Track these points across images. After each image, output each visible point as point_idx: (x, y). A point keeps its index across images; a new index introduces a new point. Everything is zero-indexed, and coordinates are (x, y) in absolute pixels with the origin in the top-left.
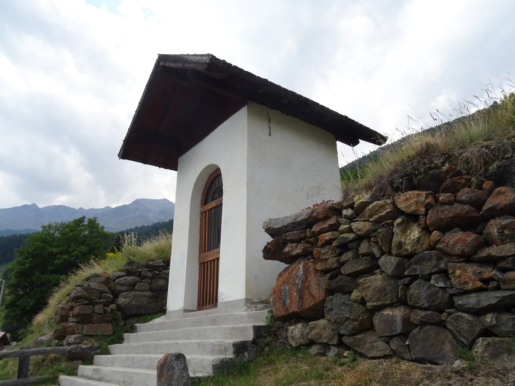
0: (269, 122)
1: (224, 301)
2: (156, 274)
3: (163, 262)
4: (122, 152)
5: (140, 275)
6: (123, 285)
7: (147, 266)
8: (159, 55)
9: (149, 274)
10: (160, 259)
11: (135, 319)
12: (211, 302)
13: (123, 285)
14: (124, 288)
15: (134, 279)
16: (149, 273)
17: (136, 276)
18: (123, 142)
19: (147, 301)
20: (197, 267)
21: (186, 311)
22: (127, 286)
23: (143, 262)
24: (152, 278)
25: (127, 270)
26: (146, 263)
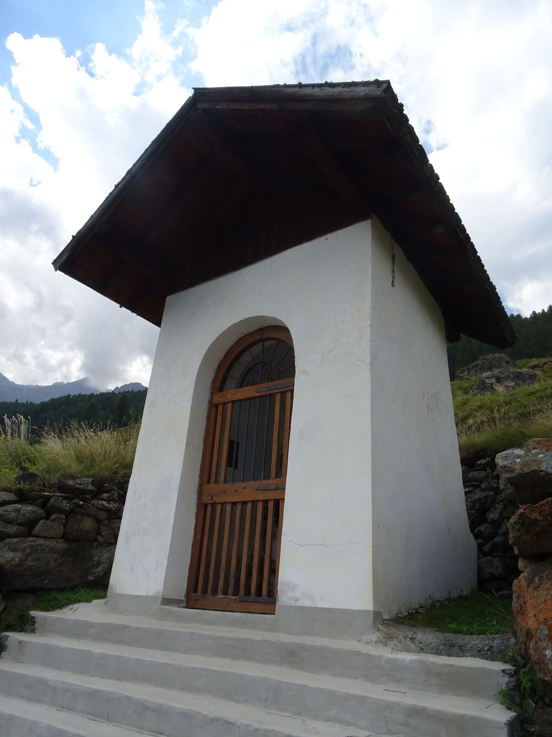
0: (393, 263)
1: (298, 604)
2: (77, 505)
3: (93, 483)
4: (64, 258)
5: (44, 503)
6: (9, 522)
7: (62, 487)
8: (195, 89)
9: (66, 505)
10: (88, 476)
11: (31, 599)
12: (231, 590)
13: (9, 522)
14: (12, 529)
15: (35, 512)
16: (65, 502)
17: (36, 505)
18: (71, 238)
19: (56, 560)
20: (194, 510)
21: (166, 601)
22: (19, 524)
23: (54, 479)
24: (69, 514)
25: (20, 490)
26: (60, 481)
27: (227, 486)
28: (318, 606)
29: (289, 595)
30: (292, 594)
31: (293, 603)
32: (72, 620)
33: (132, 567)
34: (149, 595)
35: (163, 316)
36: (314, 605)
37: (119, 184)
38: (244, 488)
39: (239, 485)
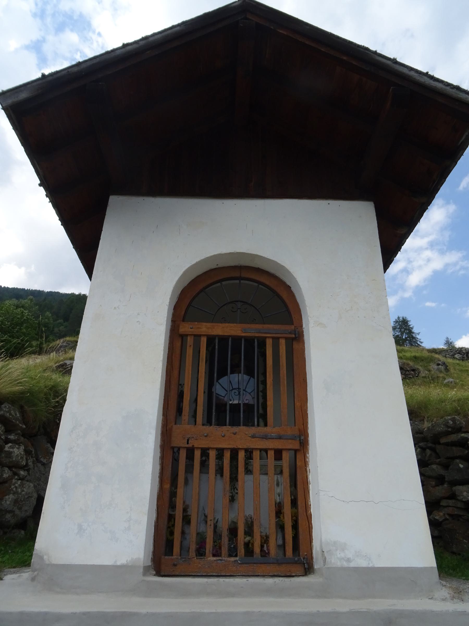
1: (352, 565)
4: (23, 95)
12: (225, 550)
27: (208, 429)
28: (376, 566)
29: (339, 556)
30: (342, 555)
31: (345, 564)
32: (11, 613)
33: (80, 527)
34: (119, 563)
35: (106, 217)
36: (371, 565)
37: (128, 45)
38: (235, 434)
39: (227, 430)
